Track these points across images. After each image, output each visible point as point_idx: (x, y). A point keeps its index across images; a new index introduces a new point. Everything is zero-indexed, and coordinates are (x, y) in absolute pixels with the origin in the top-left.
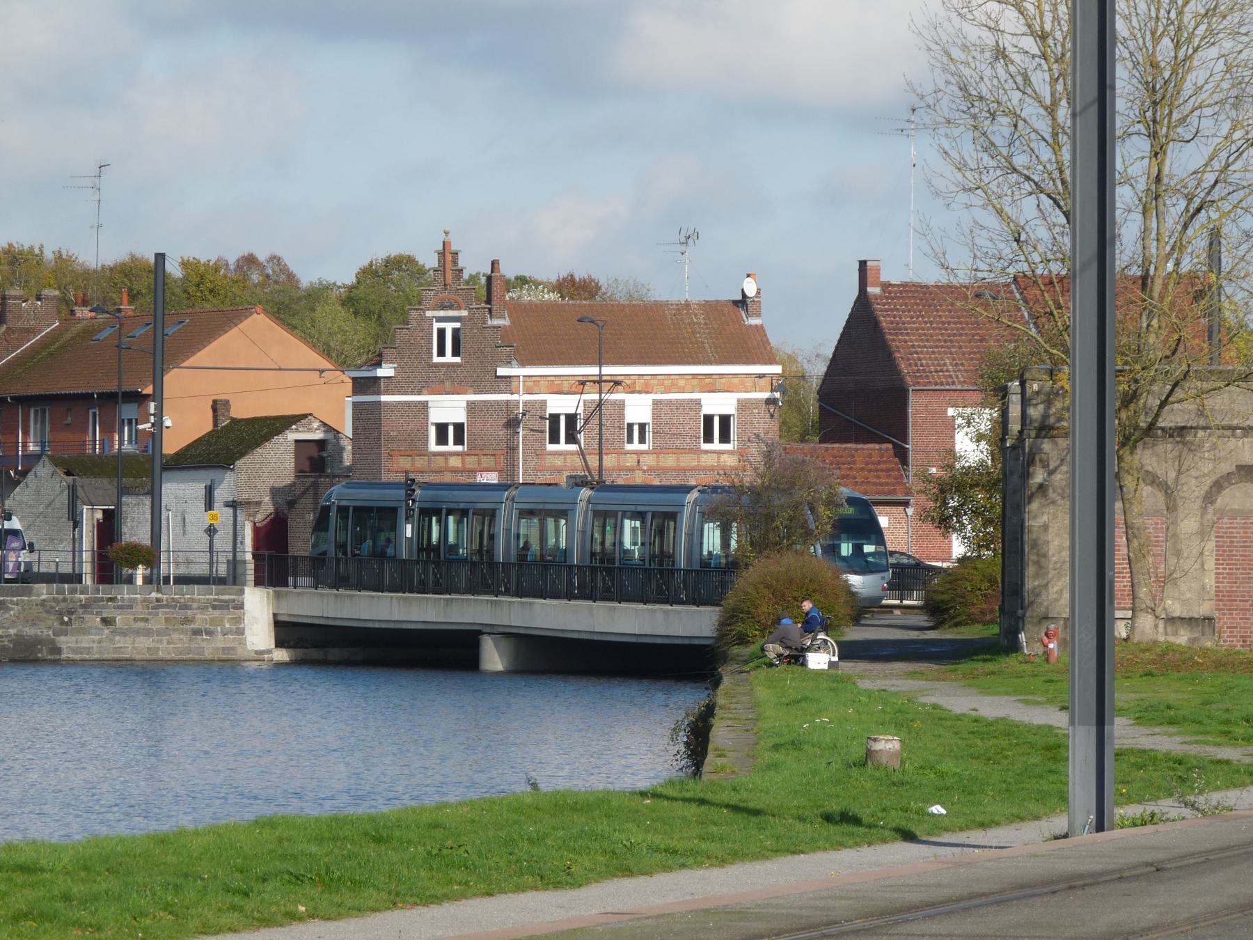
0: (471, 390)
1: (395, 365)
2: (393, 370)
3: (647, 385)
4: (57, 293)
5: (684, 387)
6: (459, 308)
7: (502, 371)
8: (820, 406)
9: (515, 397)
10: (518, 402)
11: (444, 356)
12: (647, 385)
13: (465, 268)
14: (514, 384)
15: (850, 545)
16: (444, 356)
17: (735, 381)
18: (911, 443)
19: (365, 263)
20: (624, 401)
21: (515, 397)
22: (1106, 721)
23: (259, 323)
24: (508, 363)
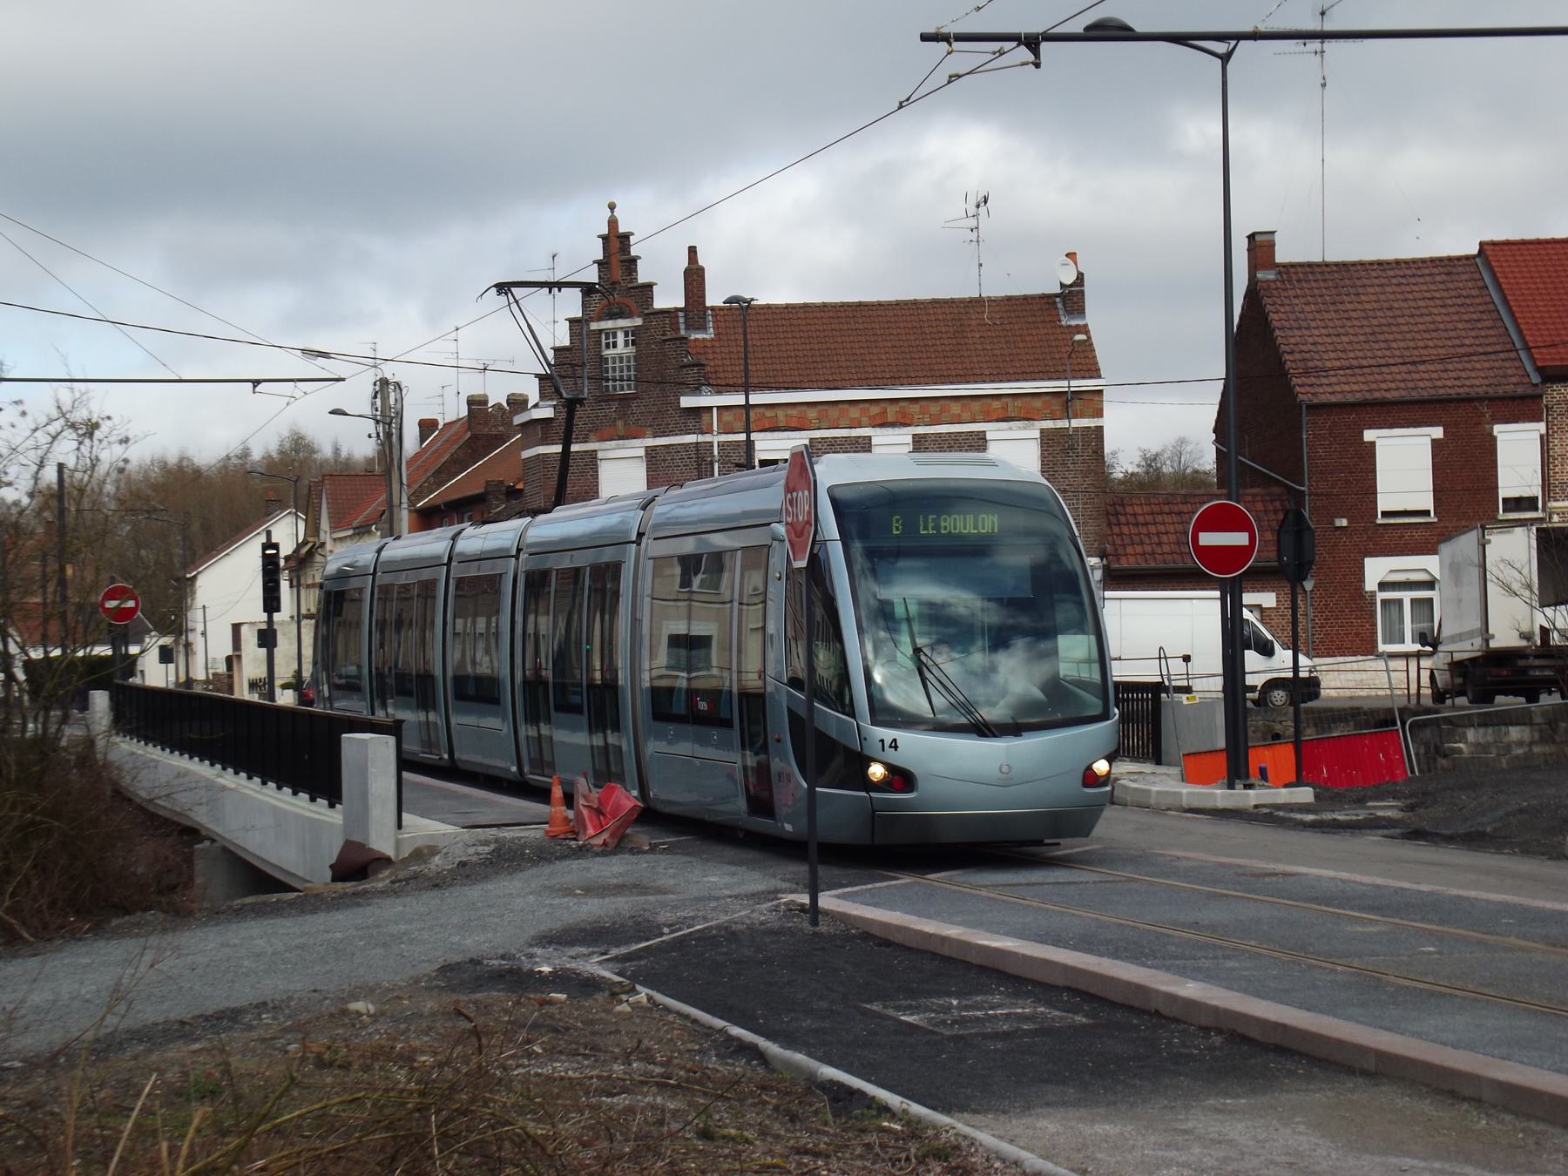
0: (649, 431)
1: (555, 403)
2: (552, 409)
3: (903, 414)
4: (181, 552)
5: (959, 415)
6: (630, 315)
7: (687, 402)
8: (1217, 448)
9: (707, 438)
10: (711, 443)
11: (1403, 642)
12: (903, 414)
13: (640, 258)
14: (705, 417)
15: (1108, 594)
16: (1403, 642)
17: (1037, 403)
18: (1307, 483)
19: (747, 296)
20: (870, 438)
21: (707, 438)
22: (529, 419)
23: (879, 597)
24: (696, 390)
